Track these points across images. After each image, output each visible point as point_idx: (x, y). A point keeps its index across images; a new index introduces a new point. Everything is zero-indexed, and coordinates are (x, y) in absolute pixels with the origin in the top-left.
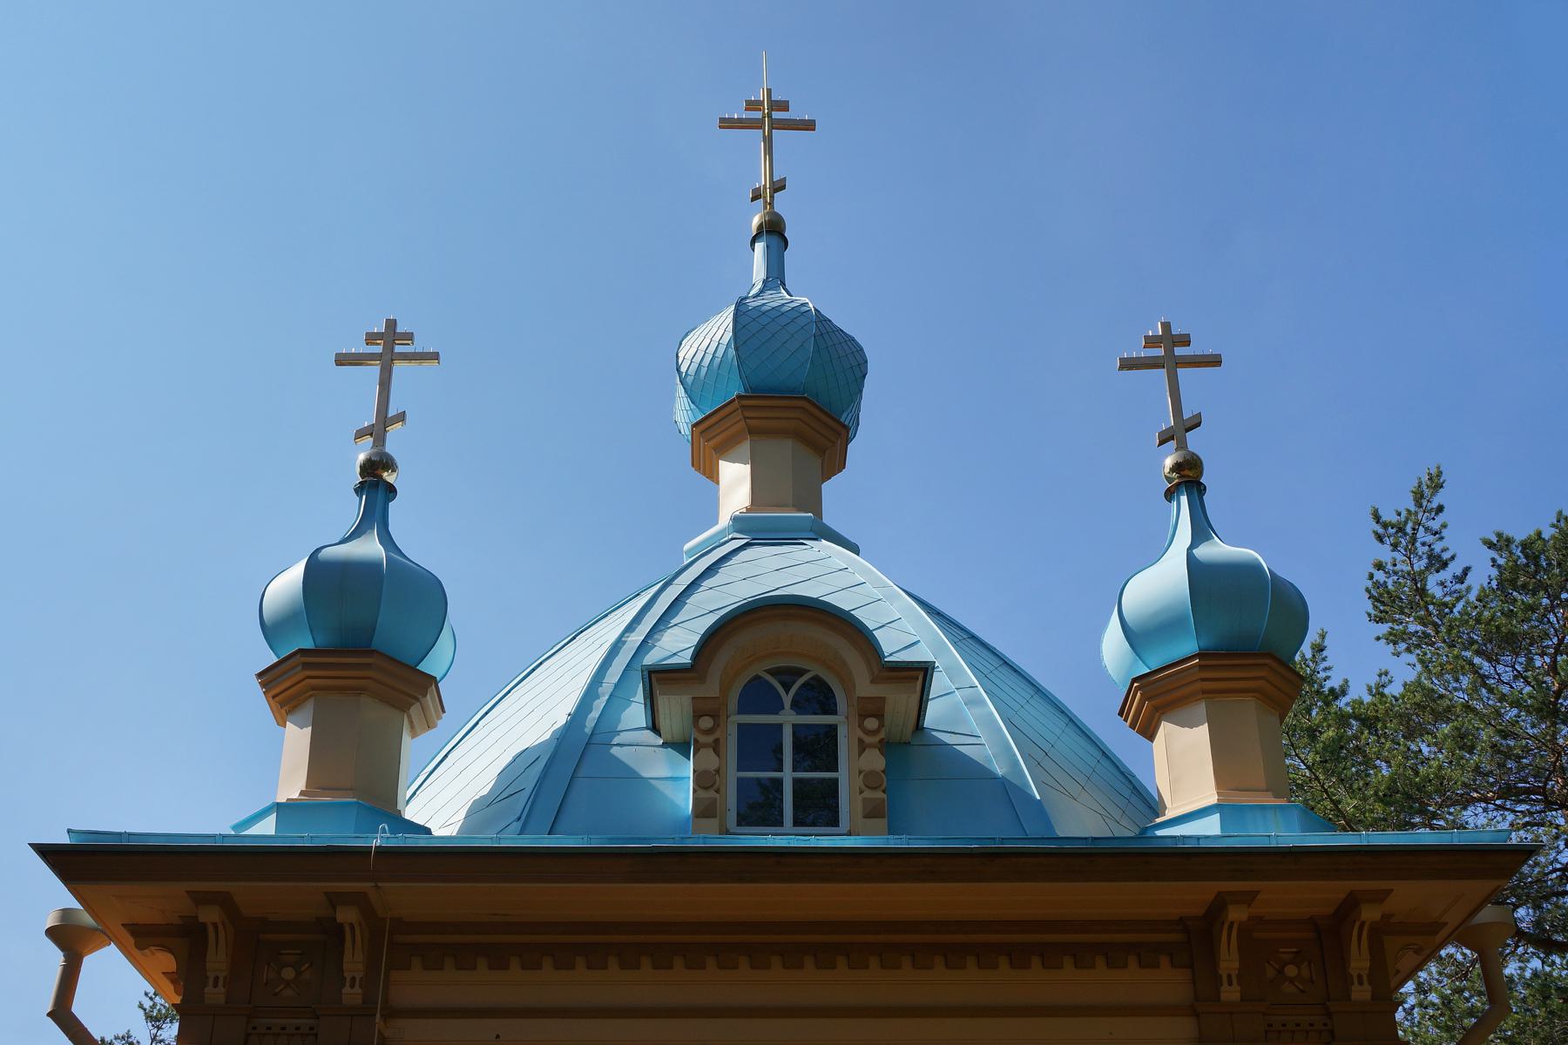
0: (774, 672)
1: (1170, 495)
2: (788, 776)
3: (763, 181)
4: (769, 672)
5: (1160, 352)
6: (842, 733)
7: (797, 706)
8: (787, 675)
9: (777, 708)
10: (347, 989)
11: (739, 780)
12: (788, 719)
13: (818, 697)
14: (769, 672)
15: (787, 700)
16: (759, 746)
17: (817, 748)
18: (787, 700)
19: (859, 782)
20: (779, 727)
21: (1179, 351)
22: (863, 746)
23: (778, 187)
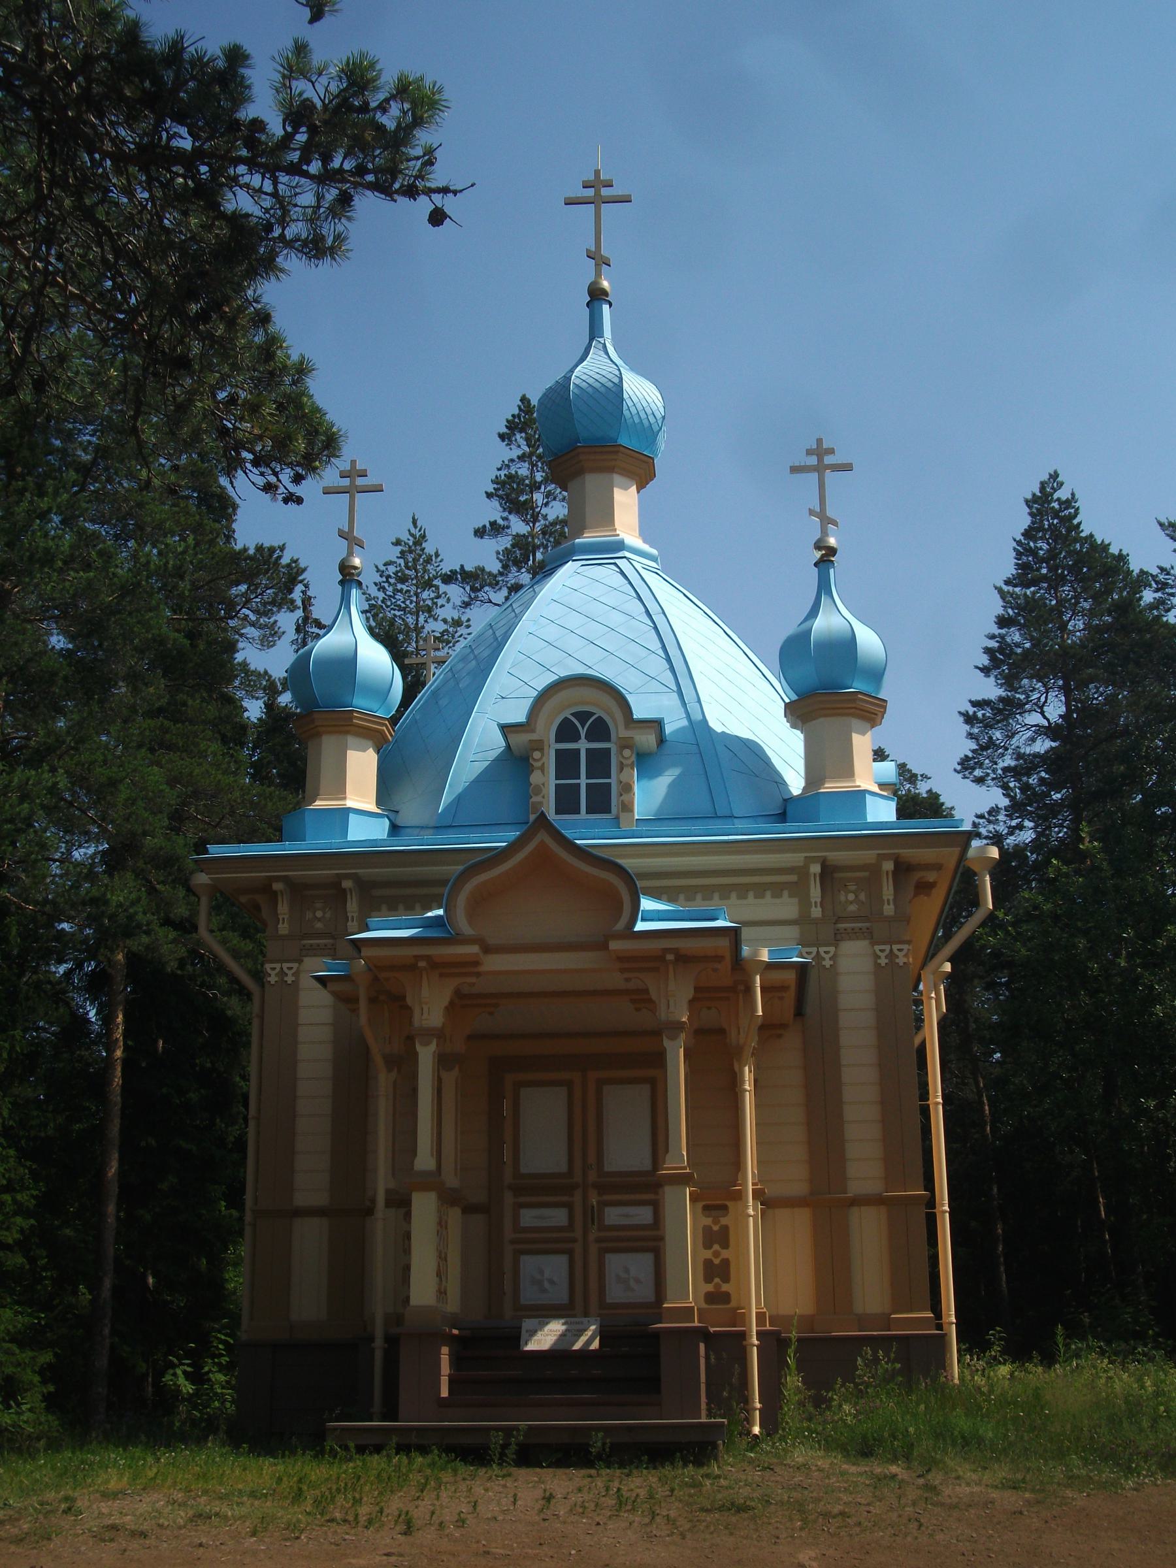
5: (813, 460)
7: (590, 737)
8: (583, 716)
9: (576, 738)
12: (583, 745)
20: (578, 751)
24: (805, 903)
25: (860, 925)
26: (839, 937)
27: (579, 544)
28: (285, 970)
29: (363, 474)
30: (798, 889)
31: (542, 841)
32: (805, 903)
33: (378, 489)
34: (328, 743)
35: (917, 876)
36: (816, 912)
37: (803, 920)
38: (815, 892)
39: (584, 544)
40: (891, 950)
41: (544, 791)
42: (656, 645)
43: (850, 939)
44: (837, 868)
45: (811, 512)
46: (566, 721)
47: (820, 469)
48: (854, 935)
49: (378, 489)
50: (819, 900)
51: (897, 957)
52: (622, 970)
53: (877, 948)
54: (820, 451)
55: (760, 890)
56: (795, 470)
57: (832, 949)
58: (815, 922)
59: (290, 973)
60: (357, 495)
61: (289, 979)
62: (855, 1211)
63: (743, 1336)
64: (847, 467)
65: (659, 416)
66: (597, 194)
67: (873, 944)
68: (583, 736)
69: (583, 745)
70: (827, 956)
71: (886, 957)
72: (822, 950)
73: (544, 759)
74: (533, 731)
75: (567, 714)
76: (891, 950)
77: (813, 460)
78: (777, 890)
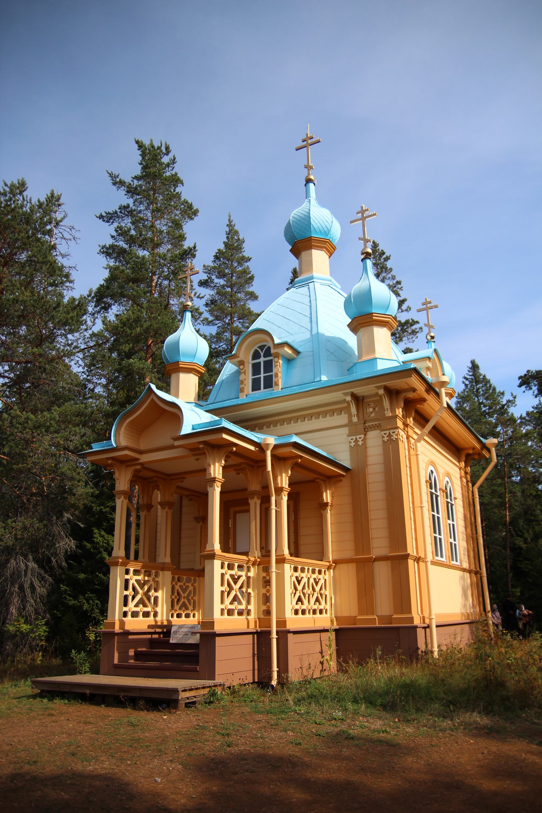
9: (259, 357)
24: (350, 416)
26: (366, 430)
27: (297, 281)
30: (347, 409)
31: (153, 399)
32: (350, 416)
33: (436, 307)
34: (173, 376)
35: (403, 395)
36: (355, 419)
37: (350, 424)
38: (354, 410)
39: (301, 280)
41: (245, 382)
42: (308, 314)
43: (371, 430)
44: (363, 398)
45: (360, 239)
47: (363, 219)
48: (373, 428)
49: (436, 307)
50: (356, 413)
51: (392, 436)
52: (194, 455)
55: (332, 412)
57: (362, 436)
58: (355, 424)
62: (376, 563)
63: (269, 633)
65: (330, 222)
66: (308, 142)
68: (262, 354)
69: (262, 360)
70: (360, 440)
72: (358, 437)
73: (245, 369)
74: (238, 357)
75: (256, 347)
78: (340, 411)
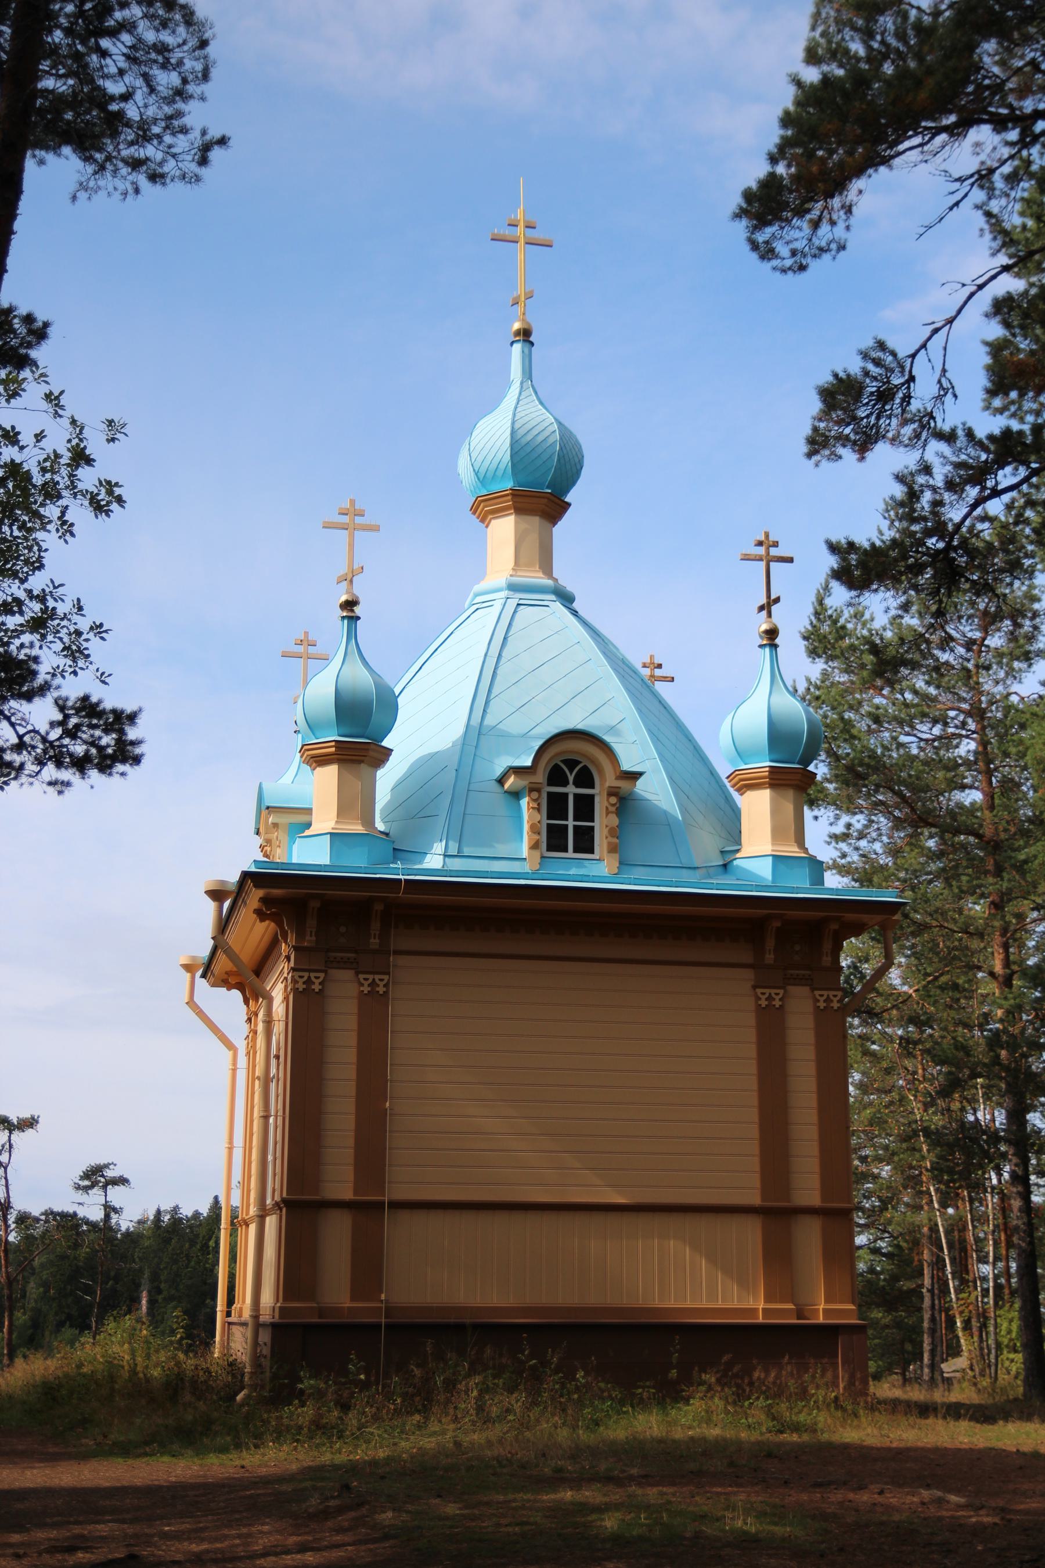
0: (565, 762)
1: (485, 508)
2: (571, 823)
3: (520, 291)
4: (562, 761)
5: (345, 519)
6: (597, 799)
7: (577, 784)
8: (571, 764)
9: (565, 783)
10: (372, 940)
11: (548, 824)
12: (571, 790)
13: (585, 779)
14: (562, 761)
15: (571, 778)
16: (556, 806)
17: (585, 808)
18: (571, 778)
19: (605, 831)
20: (566, 795)
21: (358, 520)
22: (608, 813)
23: (529, 296)
25: (803, 972)
28: (313, 979)
29: (776, 544)
40: (309, 977)
46: (556, 766)
51: (378, 986)
53: (817, 993)
54: (766, 543)
56: (746, 558)
59: (317, 981)
60: (763, 564)
61: (317, 987)
64: (375, 528)
67: (813, 990)
71: (369, 985)
76: (309, 977)
77: (761, 551)
